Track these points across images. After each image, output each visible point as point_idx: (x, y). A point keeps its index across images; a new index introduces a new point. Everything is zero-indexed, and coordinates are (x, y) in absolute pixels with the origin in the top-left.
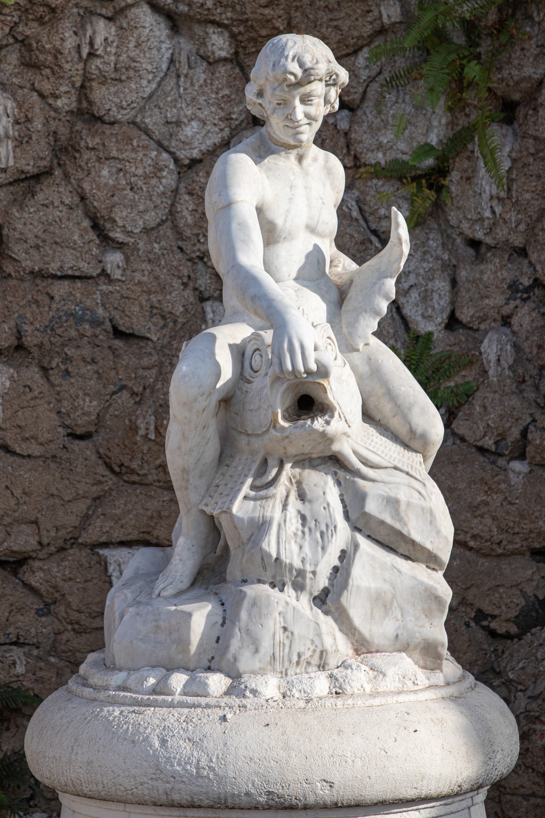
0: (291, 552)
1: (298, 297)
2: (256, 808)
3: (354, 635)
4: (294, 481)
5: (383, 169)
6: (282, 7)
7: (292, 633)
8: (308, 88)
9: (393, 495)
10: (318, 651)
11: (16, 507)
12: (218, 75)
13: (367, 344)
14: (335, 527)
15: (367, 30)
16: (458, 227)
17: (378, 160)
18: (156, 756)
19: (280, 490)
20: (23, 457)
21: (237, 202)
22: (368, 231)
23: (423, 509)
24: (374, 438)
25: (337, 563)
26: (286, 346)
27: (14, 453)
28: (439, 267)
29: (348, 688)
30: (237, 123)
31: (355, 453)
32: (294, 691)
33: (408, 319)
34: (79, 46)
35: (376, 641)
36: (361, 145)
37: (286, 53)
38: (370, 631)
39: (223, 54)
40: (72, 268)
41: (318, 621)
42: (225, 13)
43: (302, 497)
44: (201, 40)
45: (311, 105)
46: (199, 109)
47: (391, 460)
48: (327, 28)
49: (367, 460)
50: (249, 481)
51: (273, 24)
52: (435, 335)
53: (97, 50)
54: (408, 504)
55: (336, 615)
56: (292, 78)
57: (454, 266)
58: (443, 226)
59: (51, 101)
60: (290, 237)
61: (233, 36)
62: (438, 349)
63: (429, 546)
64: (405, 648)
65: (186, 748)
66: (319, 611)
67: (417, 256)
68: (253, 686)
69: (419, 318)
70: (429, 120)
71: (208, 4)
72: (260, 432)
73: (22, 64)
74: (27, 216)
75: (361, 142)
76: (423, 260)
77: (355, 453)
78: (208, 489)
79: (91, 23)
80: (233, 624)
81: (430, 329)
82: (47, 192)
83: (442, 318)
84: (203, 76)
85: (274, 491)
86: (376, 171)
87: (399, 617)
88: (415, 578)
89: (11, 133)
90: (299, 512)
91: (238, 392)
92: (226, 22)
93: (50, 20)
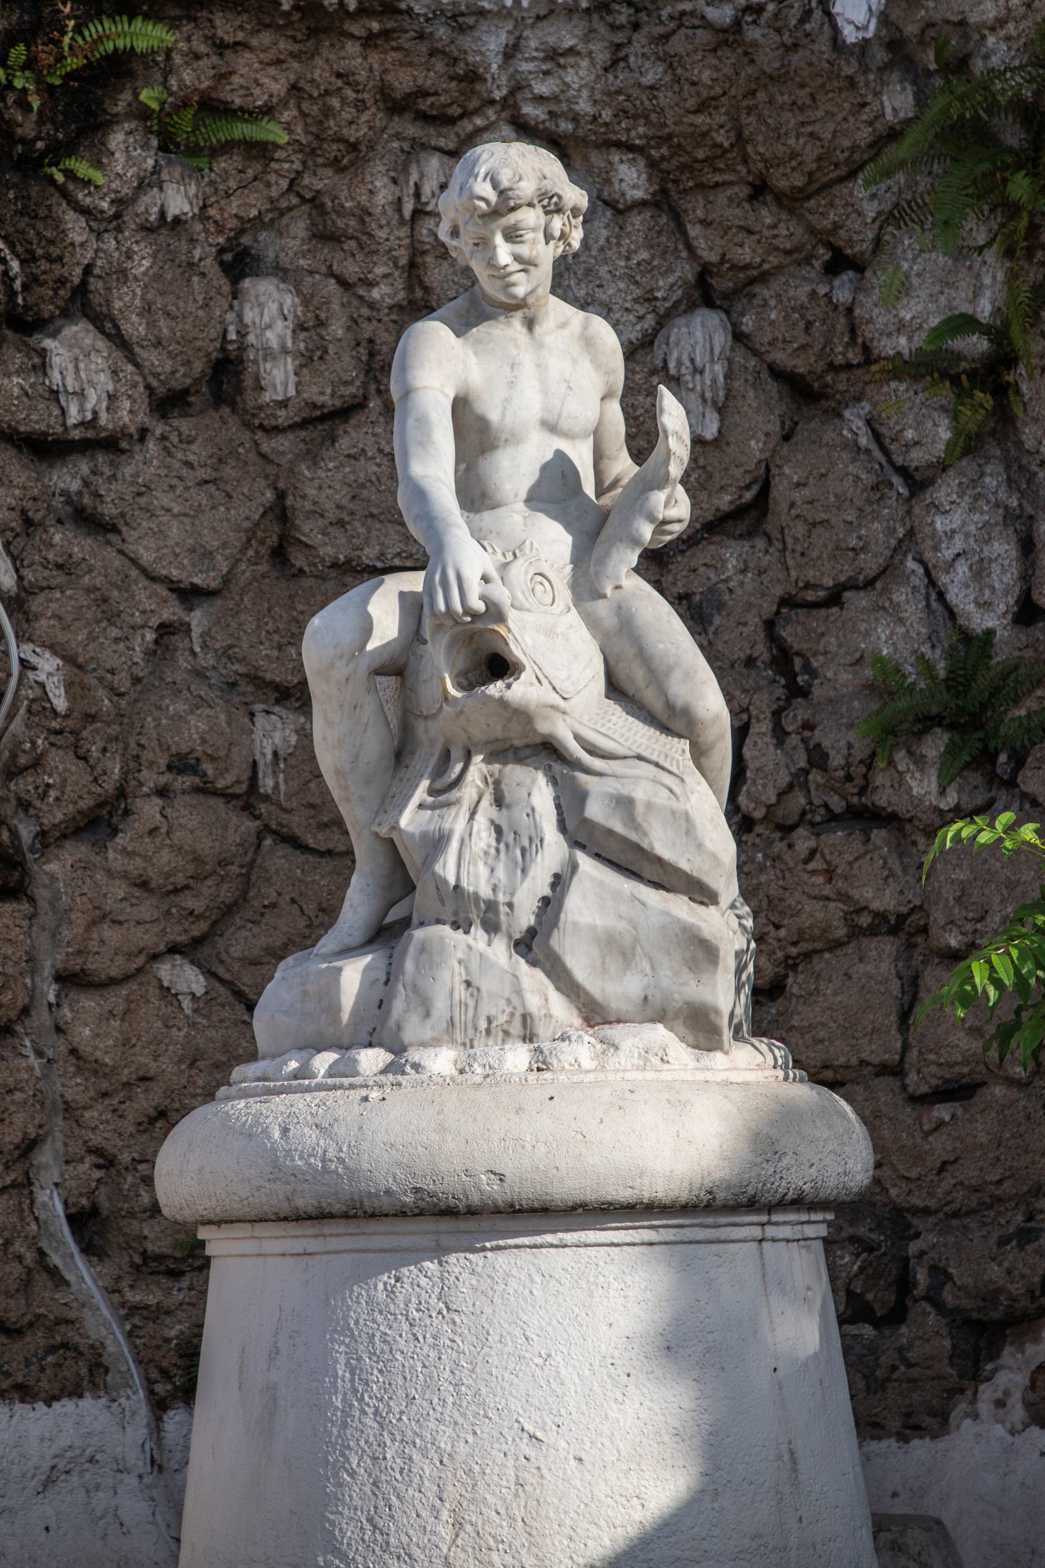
0: (477, 876)
1: (525, 525)
2: (404, 1214)
3: (578, 996)
4: (490, 780)
5: (906, 362)
6: (723, 110)
7: (478, 990)
8: (512, 218)
9: (625, 792)
10: (518, 1014)
11: (307, 931)
12: (629, 229)
13: (618, 587)
14: (542, 841)
15: (864, 136)
16: (1038, 452)
17: (900, 349)
18: (274, 1150)
19: (468, 792)
20: (321, 854)
21: (418, 389)
22: (888, 469)
23: (673, 812)
24: (614, 718)
25: (547, 891)
26: (437, 577)
27: (305, 848)
28: (1000, 519)
29: (555, 1062)
30: (667, 305)
31: (577, 737)
32: (476, 1066)
33: (956, 610)
34: (399, 199)
35: (613, 1005)
36: (871, 326)
37: (476, 171)
38: (603, 989)
39: (639, 194)
40: (399, 554)
41: (517, 973)
42: (635, 128)
43: (499, 801)
44: (604, 175)
45: (522, 242)
46: (599, 286)
47: (634, 747)
48: (797, 138)
49: (594, 746)
50: (425, 783)
51: (712, 138)
52: (998, 634)
53: (427, 203)
54: (649, 805)
55: (547, 965)
56: (482, 205)
57: (1031, 517)
58: (1013, 453)
59: (361, 292)
60: (514, 439)
61: (652, 164)
62: (1001, 655)
63: (684, 865)
64: (661, 1016)
65: (311, 1136)
66: (522, 961)
67: (963, 504)
68: (416, 1059)
69: (971, 608)
70: (978, 276)
71: (604, 115)
72: (434, 711)
73: (314, 236)
74: (323, 475)
75: (870, 321)
76: (972, 509)
77: (577, 737)
78: (383, 802)
79: (418, 162)
80: (397, 978)
81: (990, 624)
82: (354, 435)
83: (1005, 604)
84: (605, 233)
85: (458, 794)
86: (895, 367)
87: (648, 970)
88: (667, 913)
89: (289, 344)
90: (492, 822)
91: (412, 659)
92: (637, 142)
93: (352, 163)
